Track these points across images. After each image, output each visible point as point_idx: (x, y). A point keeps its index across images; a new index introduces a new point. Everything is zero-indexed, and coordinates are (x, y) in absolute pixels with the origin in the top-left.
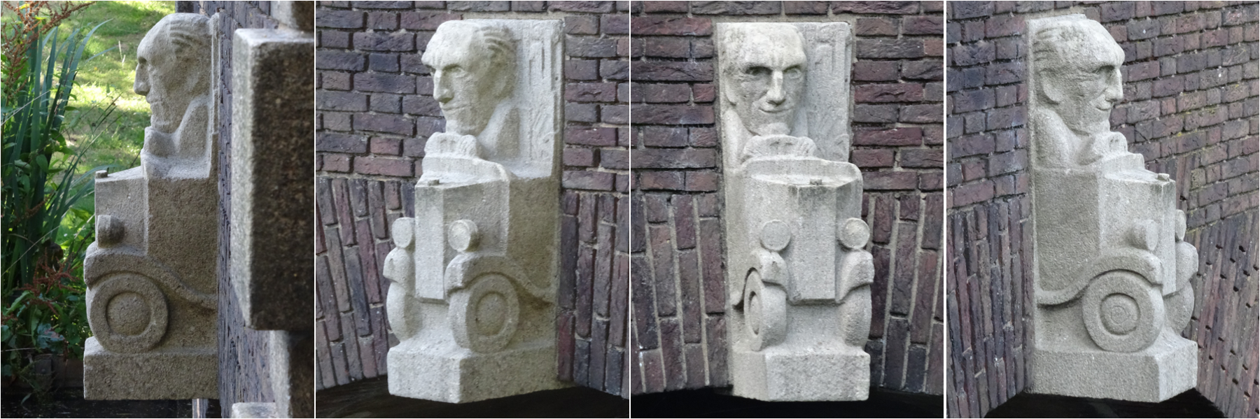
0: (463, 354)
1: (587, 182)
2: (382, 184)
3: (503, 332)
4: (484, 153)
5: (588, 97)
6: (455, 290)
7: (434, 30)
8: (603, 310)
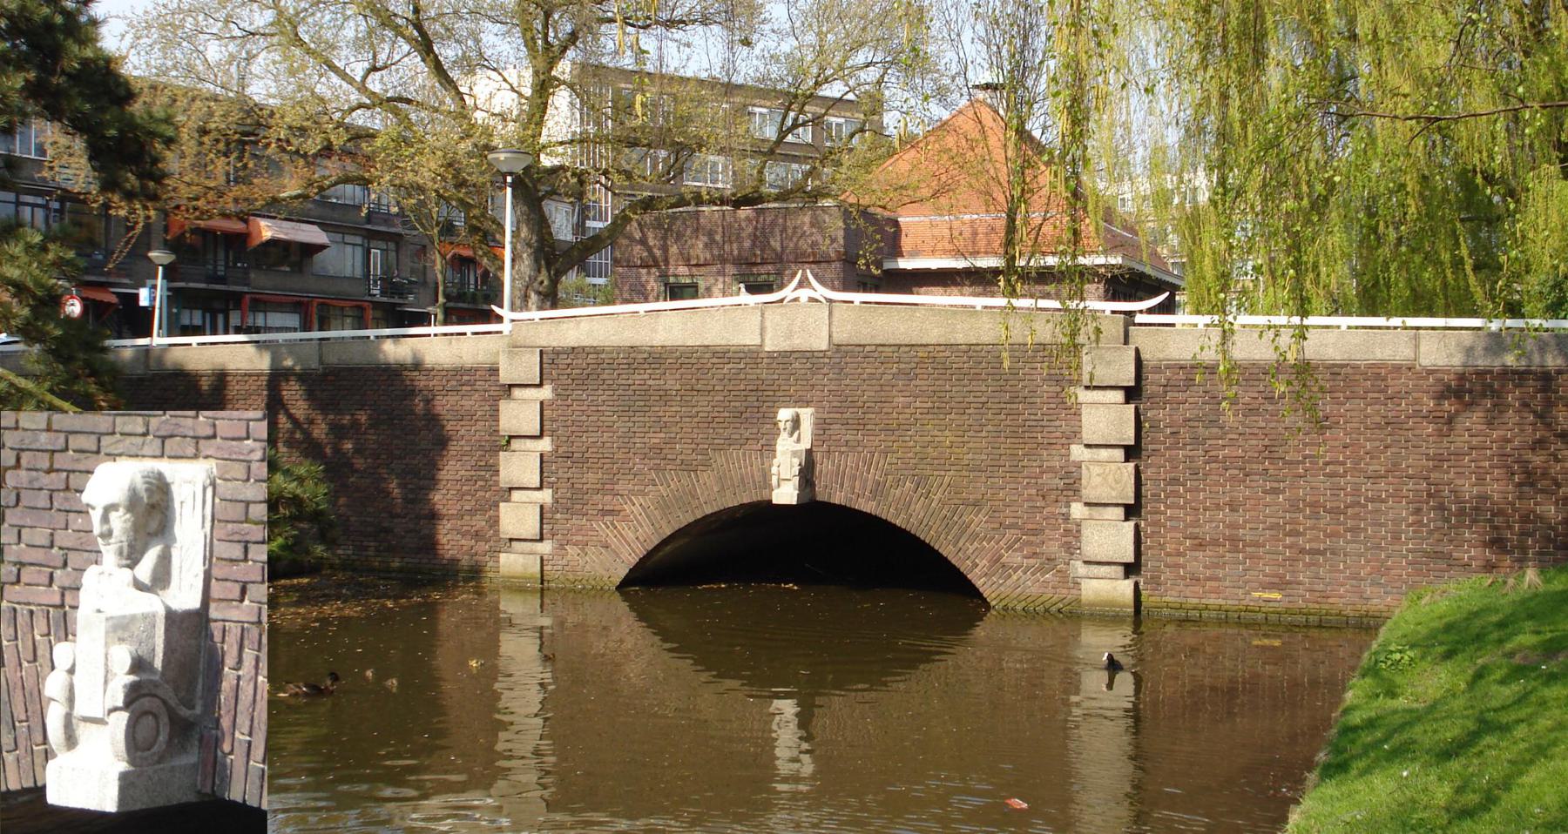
0: (123, 766)
1: (234, 614)
2: (32, 612)
3: (155, 749)
4: (139, 586)
5: (236, 537)
6: (116, 709)
7: (92, 472)
8: (246, 730)
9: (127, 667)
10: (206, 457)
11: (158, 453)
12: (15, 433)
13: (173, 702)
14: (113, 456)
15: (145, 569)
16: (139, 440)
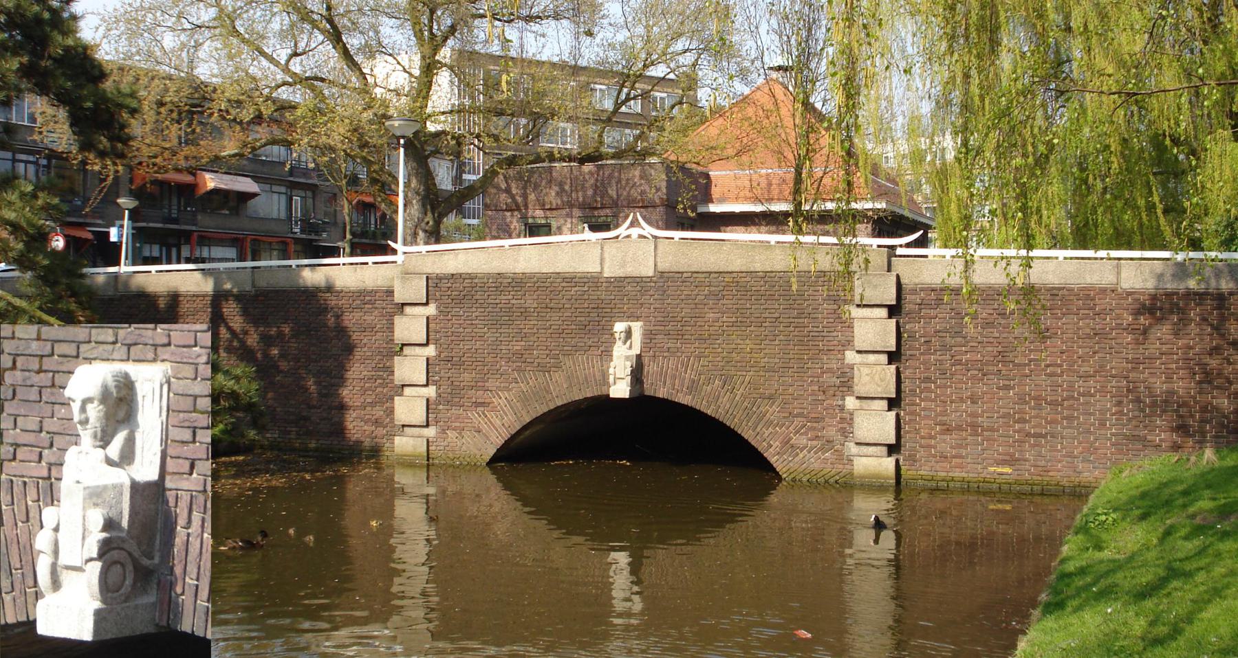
0: (97, 604)
1: (185, 485)
2: (25, 483)
3: (122, 591)
4: (110, 462)
5: (187, 424)
6: (91, 560)
7: (72, 373)
8: (194, 576)
9: (100, 526)
10: (163, 361)
11: (125, 357)
12: (12, 342)
13: (136, 554)
14: (89, 360)
15: (114, 449)
16: (110, 347)
